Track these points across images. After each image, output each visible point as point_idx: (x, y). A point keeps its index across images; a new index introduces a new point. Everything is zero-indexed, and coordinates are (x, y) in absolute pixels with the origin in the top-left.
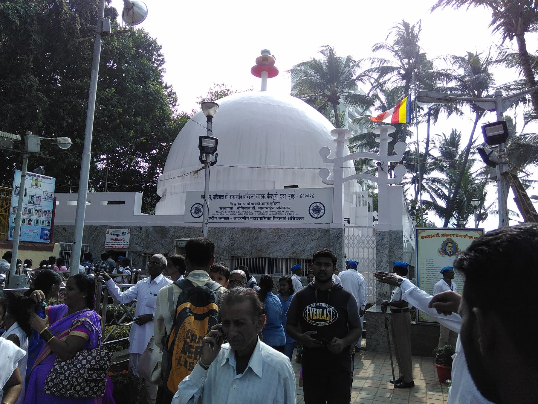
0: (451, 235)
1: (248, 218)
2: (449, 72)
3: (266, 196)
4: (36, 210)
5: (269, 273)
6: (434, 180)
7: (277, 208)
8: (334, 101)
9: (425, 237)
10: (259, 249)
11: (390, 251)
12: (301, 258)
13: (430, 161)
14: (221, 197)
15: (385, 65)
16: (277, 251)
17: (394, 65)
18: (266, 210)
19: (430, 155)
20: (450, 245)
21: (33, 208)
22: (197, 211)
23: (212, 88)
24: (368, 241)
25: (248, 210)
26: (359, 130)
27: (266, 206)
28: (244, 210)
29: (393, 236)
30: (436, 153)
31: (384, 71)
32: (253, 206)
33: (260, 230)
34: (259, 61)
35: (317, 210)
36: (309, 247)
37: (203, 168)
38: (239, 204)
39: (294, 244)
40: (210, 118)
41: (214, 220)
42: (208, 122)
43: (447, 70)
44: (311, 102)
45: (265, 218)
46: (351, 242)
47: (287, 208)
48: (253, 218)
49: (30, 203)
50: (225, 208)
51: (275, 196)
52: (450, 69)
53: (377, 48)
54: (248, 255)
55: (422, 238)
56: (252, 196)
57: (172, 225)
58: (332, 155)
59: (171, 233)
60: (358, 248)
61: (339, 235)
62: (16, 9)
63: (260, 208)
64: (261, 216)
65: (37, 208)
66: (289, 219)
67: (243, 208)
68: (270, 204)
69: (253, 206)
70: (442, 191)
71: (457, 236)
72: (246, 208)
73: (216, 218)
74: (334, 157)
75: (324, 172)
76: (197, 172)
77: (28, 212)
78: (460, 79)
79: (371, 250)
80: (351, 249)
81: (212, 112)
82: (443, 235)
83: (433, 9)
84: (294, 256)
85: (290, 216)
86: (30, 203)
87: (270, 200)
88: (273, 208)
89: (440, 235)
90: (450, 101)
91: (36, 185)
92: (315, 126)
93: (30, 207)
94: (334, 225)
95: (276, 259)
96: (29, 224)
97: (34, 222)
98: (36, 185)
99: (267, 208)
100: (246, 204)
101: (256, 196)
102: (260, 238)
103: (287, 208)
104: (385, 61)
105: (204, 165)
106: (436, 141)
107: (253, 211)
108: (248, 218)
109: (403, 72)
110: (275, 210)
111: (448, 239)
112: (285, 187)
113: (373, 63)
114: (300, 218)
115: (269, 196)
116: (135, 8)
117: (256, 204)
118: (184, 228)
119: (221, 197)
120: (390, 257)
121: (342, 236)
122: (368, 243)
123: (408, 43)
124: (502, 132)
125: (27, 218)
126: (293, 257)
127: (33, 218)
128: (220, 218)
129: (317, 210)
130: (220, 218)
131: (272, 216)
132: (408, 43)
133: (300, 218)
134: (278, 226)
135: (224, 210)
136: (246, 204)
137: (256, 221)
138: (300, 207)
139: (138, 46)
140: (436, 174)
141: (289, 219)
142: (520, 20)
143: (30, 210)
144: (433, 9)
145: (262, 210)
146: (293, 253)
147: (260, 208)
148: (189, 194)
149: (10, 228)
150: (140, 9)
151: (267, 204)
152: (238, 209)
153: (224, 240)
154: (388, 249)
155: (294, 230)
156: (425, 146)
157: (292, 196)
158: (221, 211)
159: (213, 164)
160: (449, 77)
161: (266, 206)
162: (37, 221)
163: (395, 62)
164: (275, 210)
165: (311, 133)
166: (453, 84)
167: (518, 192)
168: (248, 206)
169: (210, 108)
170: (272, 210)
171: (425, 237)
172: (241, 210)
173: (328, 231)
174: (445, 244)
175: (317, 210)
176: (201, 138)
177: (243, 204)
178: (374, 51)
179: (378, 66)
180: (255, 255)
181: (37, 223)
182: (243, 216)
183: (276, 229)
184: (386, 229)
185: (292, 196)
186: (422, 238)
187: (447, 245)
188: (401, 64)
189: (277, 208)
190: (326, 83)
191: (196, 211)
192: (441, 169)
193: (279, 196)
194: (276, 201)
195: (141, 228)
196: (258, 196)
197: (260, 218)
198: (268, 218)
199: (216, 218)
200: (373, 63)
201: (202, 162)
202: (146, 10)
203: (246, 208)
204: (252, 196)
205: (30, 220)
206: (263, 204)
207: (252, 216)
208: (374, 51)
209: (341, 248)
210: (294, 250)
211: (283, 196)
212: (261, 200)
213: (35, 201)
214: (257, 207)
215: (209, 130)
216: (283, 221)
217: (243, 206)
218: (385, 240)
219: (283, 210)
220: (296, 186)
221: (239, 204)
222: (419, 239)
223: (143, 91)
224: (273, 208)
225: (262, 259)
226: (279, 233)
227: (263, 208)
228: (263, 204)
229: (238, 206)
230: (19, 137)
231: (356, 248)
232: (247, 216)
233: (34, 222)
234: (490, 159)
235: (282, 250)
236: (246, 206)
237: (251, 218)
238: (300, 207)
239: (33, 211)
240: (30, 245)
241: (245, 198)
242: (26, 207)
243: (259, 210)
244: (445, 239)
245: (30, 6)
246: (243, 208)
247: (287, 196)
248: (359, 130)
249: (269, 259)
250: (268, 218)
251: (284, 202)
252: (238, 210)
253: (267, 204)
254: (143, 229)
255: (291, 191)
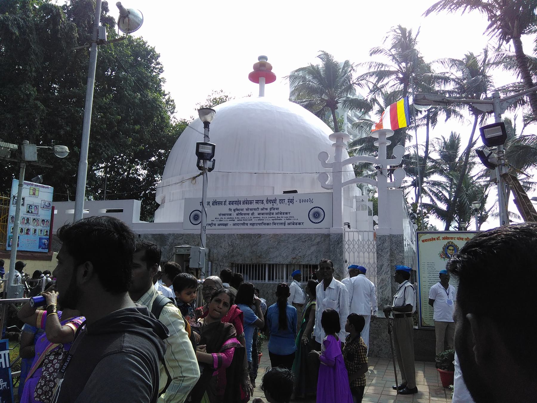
0: (452, 238)
1: (247, 224)
2: (447, 75)
3: (265, 202)
4: (34, 219)
5: (269, 279)
6: (435, 184)
7: (277, 214)
8: (332, 105)
9: (426, 240)
10: (259, 255)
11: (391, 255)
12: (301, 263)
13: (429, 164)
14: (220, 203)
15: (383, 69)
16: (277, 257)
17: (392, 69)
18: (265, 216)
19: (430, 158)
20: (451, 248)
21: (31, 217)
22: (196, 217)
23: (211, 95)
24: (369, 246)
25: (247, 216)
26: (358, 134)
27: (265, 211)
28: (243, 216)
29: (394, 239)
30: (435, 156)
31: (382, 75)
32: (252, 212)
33: (260, 236)
34: (256, 67)
35: (316, 215)
36: (309, 252)
37: (201, 174)
38: (238, 210)
39: (294, 249)
40: (207, 124)
41: (214, 227)
42: (205, 128)
43: (445, 73)
44: (309, 107)
45: (265, 224)
46: (351, 246)
47: (286, 213)
48: (253, 224)
49: (28, 212)
50: (224, 215)
51: (274, 201)
52: (447, 73)
53: (375, 52)
54: (248, 262)
55: (423, 241)
56: (251, 202)
57: (171, 233)
58: (330, 160)
59: (170, 240)
60: (359, 253)
61: (339, 239)
62: (15, 20)
63: (259, 214)
64: (261, 222)
65: (35, 217)
66: (289, 224)
67: (242, 214)
68: (269, 209)
69: (252, 212)
70: (443, 194)
71: (458, 239)
72: (245, 214)
73: (215, 225)
74: (333, 161)
75: (323, 176)
76: (194, 178)
77: (26, 222)
78: (457, 81)
79: (371, 254)
80: (352, 254)
81: (208, 118)
82: (444, 238)
83: (428, 12)
84: (294, 261)
85: (289, 221)
86: (28, 212)
87: (270, 206)
88: (273, 214)
89: (441, 238)
90: (447, 104)
91: (34, 194)
92: (314, 129)
93: (28, 216)
94: (334, 230)
95: (276, 264)
96: (27, 233)
97: (32, 232)
98: (34, 194)
99: (267, 214)
100: (245, 210)
101: (255, 202)
102: (259, 244)
103: (286, 213)
104: (383, 65)
105: (201, 171)
106: (435, 145)
107: (252, 217)
108: (247, 224)
109: (401, 76)
110: (274, 215)
111: (449, 243)
112: (285, 192)
113: (370, 67)
114: (300, 224)
115: (268, 201)
116: (130, 16)
117: (255, 209)
118: (183, 235)
119: (220, 203)
120: (391, 261)
121: (342, 241)
122: (369, 247)
123: (405, 46)
124: (500, 133)
125: (25, 227)
126: (293, 262)
127: (31, 227)
128: (219, 225)
129: (316, 215)
130: (219, 225)
131: (271, 222)
132: (405, 46)
133: (300, 224)
134: (278, 232)
135: (223, 217)
136: (245, 210)
137: (255, 227)
138: (300, 212)
139: (136, 54)
140: (436, 177)
141: (289, 224)
142: (516, 22)
143: (28, 219)
144: (428, 12)
145: (261, 216)
146: (294, 259)
147: (259, 214)
148: (188, 201)
149: (8, 238)
150: (136, 16)
151: (267, 209)
152: (237, 215)
153: (223, 246)
154: (389, 253)
155: (294, 236)
156: (425, 149)
157: (291, 201)
158: (220, 217)
159: (210, 170)
160: (446, 80)
161: (265, 211)
162: (35, 230)
163: (394, 67)
164: (274, 215)
165: (309, 138)
166: (451, 86)
167: (518, 193)
168: (247, 212)
169: (207, 114)
170: (272, 216)
171: (426, 240)
172: (240, 216)
173: (328, 235)
174: (446, 248)
175: (316, 215)
176: (198, 144)
177: (242, 210)
178: (371, 55)
179: (376, 70)
180: (255, 261)
181: (35, 232)
182: (242, 222)
183: (275, 235)
184: (387, 233)
185: (291, 201)
186: (423, 241)
187: (448, 248)
188: (398, 68)
189: (277, 214)
190: (324, 88)
191: (195, 217)
192: (441, 172)
193: (278, 201)
194: (275, 206)
195: (139, 235)
196: (257, 202)
197: (260, 224)
198: (268, 224)
199: (215, 225)
200: (370, 67)
201: (200, 168)
202: (142, 18)
203: (245, 214)
204: (251, 202)
205: (28, 230)
206: (262, 209)
207: (251, 222)
208: (371, 55)
209: (342, 253)
210: (294, 256)
211: (282, 201)
212: (260, 206)
213: (33, 210)
214: (256, 212)
215: (206, 136)
216: (283, 226)
217: (242, 212)
218: (386, 244)
219: (282, 215)
220: (295, 192)
221: (238, 210)
222: (420, 242)
223: (140, 99)
224: (273, 214)
225: (262, 265)
226: (279, 239)
227: (263, 214)
228: (262, 209)
229: (237, 212)
230: (16, 146)
231: (356, 254)
232: (246, 222)
233: (32, 232)
234: (489, 160)
235: (281, 256)
236: (245, 212)
237: (251, 224)
238: (300, 212)
239: (31, 221)
240: (28, 254)
241: (243, 203)
242: (24, 216)
243: (259, 216)
244: (446, 242)
245: (29, 17)
246: (242, 214)
247: (286, 201)
248: (358, 134)
249: (269, 265)
250: (268, 224)
251: (283, 208)
252: (237, 216)
253: (267, 209)
254: (142, 237)
255: (291, 196)
